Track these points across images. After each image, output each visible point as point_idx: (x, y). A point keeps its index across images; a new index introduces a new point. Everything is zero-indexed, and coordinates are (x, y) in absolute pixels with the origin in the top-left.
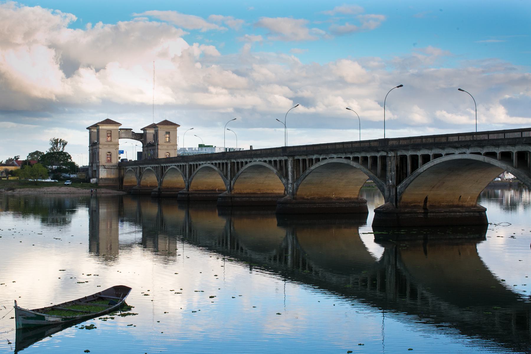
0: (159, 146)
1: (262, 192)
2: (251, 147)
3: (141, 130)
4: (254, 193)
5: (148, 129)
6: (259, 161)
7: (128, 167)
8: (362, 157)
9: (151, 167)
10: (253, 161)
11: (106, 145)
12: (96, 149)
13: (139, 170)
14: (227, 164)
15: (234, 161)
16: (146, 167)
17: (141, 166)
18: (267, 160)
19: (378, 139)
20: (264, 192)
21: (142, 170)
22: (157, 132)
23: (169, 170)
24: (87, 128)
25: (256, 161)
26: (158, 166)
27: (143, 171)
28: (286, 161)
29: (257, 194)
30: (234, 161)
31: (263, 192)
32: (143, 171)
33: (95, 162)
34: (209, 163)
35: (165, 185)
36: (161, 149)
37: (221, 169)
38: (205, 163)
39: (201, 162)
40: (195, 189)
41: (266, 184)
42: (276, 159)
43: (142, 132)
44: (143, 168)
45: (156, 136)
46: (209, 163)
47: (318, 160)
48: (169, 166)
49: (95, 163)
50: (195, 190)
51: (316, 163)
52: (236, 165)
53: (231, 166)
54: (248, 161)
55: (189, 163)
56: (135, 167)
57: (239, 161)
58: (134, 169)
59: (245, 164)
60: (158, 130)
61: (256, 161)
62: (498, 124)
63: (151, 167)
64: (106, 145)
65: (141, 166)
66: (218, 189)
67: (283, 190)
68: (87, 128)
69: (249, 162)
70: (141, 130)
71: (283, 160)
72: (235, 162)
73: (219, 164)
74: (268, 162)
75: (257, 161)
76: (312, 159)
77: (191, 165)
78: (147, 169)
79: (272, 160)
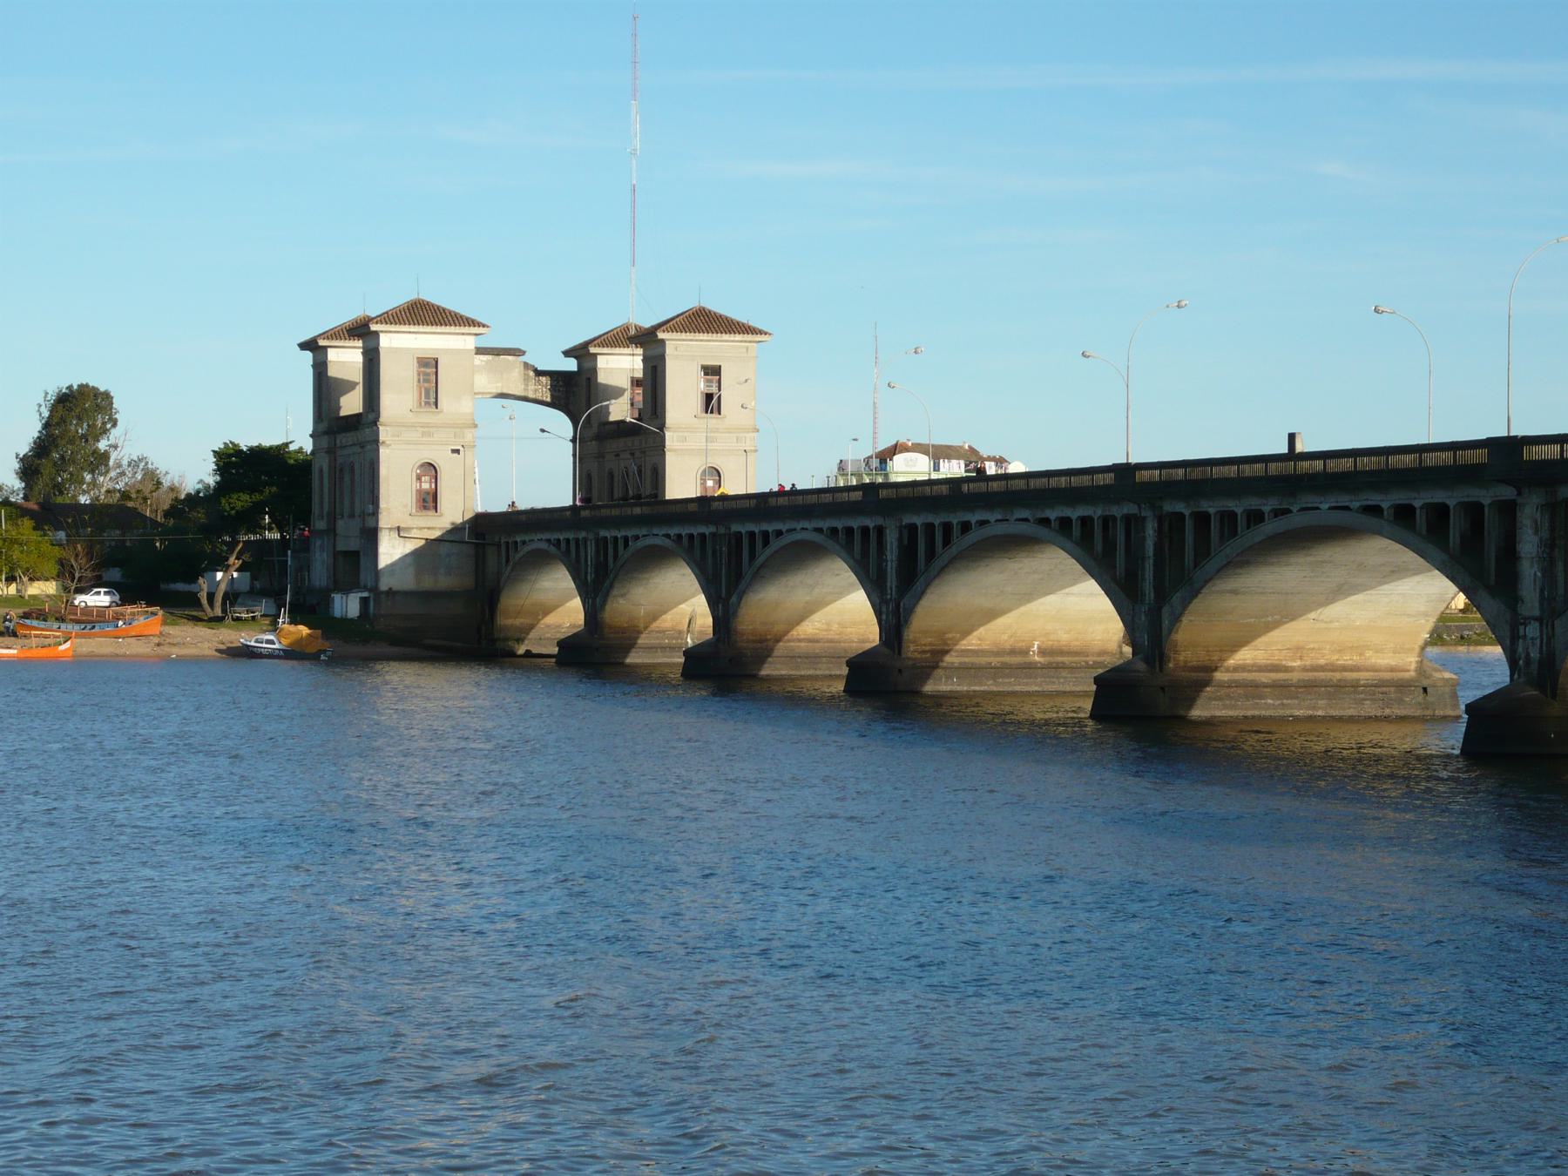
0: (799, 487)
1: (1308, 663)
2: (1292, 438)
3: (567, 353)
4: (1272, 665)
5: (605, 350)
6: (1330, 508)
7: (527, 538)
8: (1460, 504)
9: (667, 536)
10: (1295, 509)
11: (413, 426)
12: (356, 449)
13: (597, 552)
14: (880, 531)
15: (1180, 507)
16: (637, 538)
17: (603, 533)
18: (1385, 505)
19: (1484, 437)
20: (1322, 662)
21: (611, 551)
22: (659, 369)
23: (776, 552)
24: (304, 346)
25: (1317, 508)
26: (714, 535)
27: (616, 557)
28: (1508, 510)
29: (1287, 669)
30: (1180, 507)
31: (1315, 662)
32: (616, 557)
33: (347, 511)
34: (1026, 520)
35: (751, 627)
36: (675, 450)
37: (1099, 546)
38: (999, 517)
39: (798, 521)
40: (930, 644)
41: (1331, 622)
42: (930, 518)
43: (571, 365)
44: (759, 542)
45: (653, 382)
46: (1026, 520)
47: (983, 523)
48: (779, 533)
49: (352, 516)
50: (928, 648)
51: (1248, 528)
52: (1189, 525)
53: (1160, 531)
54: (1266, 509)
55: (902, 520)
56: (571, 536)
57: (1212, 511)
58: (563, 545)
59: (959, 532)
60: (662, 358)
61: (1317, 508)
62: (391, 332)
63: (667, 536)
64: (413, 426)
65: (603, 533)
66: (1039, 648)
67: (1413, 649)
68: (304, 346)
69: (977, 522)
70: (567, 353)
71: (871, 527)
72: (1187, 512)
73: (1085, 521)
74: (1058, 522)
75: (1325, 506)
76: (1233, 515)
77: (913, 528)
78: (646, 547)
79: (1417, 504)
